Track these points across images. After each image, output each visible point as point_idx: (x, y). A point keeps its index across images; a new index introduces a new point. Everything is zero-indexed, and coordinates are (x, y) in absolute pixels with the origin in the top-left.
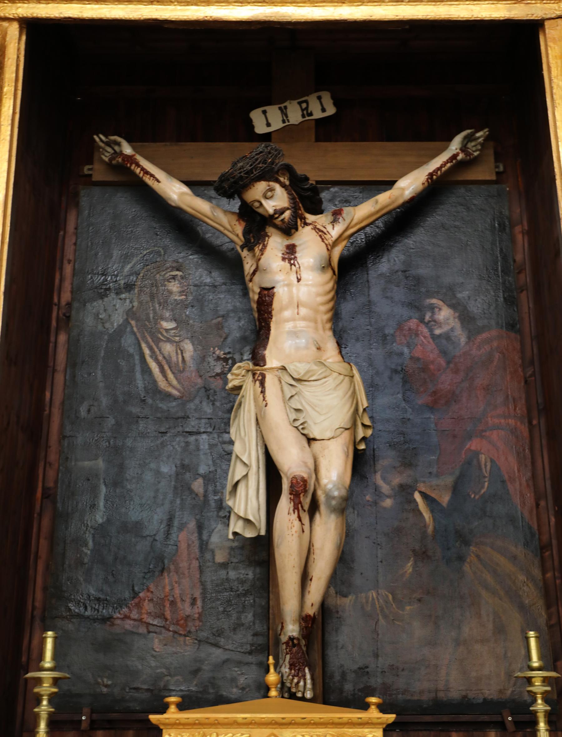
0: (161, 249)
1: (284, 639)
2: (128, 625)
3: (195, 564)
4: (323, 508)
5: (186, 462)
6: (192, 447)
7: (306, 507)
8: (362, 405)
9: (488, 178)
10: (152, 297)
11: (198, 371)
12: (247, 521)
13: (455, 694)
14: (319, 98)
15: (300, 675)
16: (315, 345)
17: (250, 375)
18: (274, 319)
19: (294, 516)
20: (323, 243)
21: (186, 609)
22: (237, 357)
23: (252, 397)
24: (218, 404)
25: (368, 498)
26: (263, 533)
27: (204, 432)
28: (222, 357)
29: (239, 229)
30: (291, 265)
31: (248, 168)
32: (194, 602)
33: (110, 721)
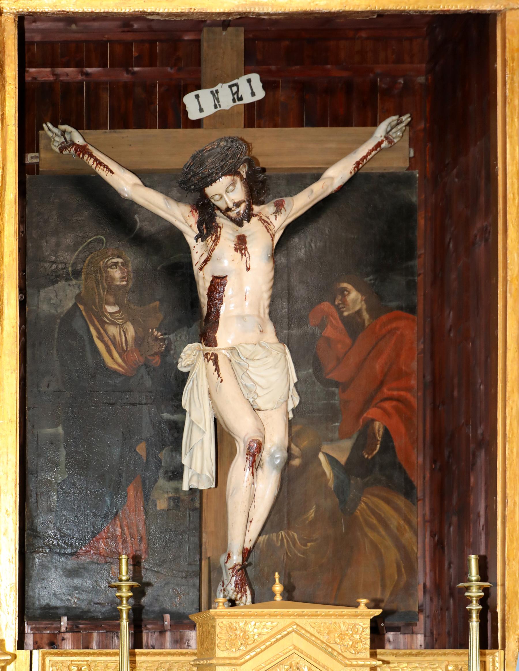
0: (103, 237)
8: (293, 380)
15: (243, 591)
16: (259, 328)
20: (268, 233)
23: (204, 374)
27: (145, 404)
28: (160, 337)
30: (242, 255)
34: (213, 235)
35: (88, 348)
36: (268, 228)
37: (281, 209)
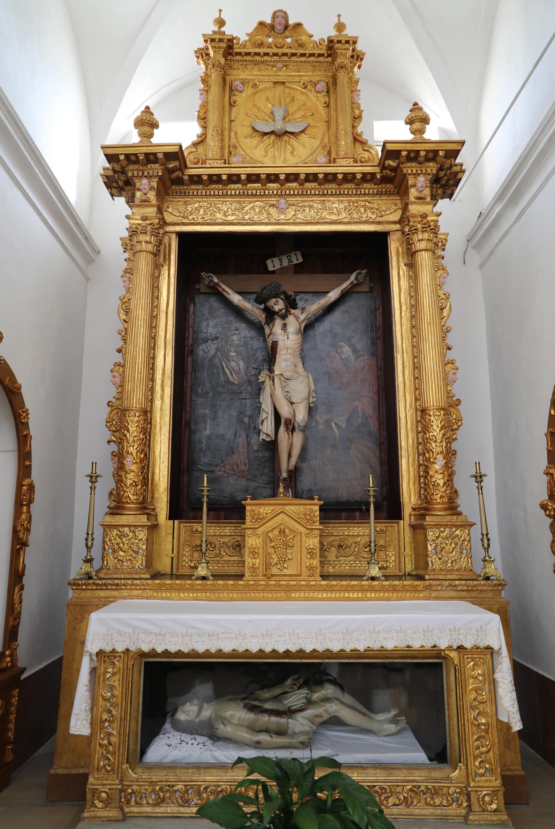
1: (281, 478)
2: (221, 473)
3: (246, 450)
4: (297, 430)
5: (241, 411)
6: (243, 405)
7: (291, 429)
9: (366, 290)
10: (226, 342)
11: (245, 373)
12: (267, 435)
13: (344, 499)
14: (296, 254)
17: (268, 377)
19: (286, 433)
21: (243, 468)
22: (261, 367)
24: (254, 387)
25: (313, 425)
26: (273, 439)
29: (264, 316)
31: (268, 293)
32: (245, 465)
33: (215, 508)
35: (221, 372)
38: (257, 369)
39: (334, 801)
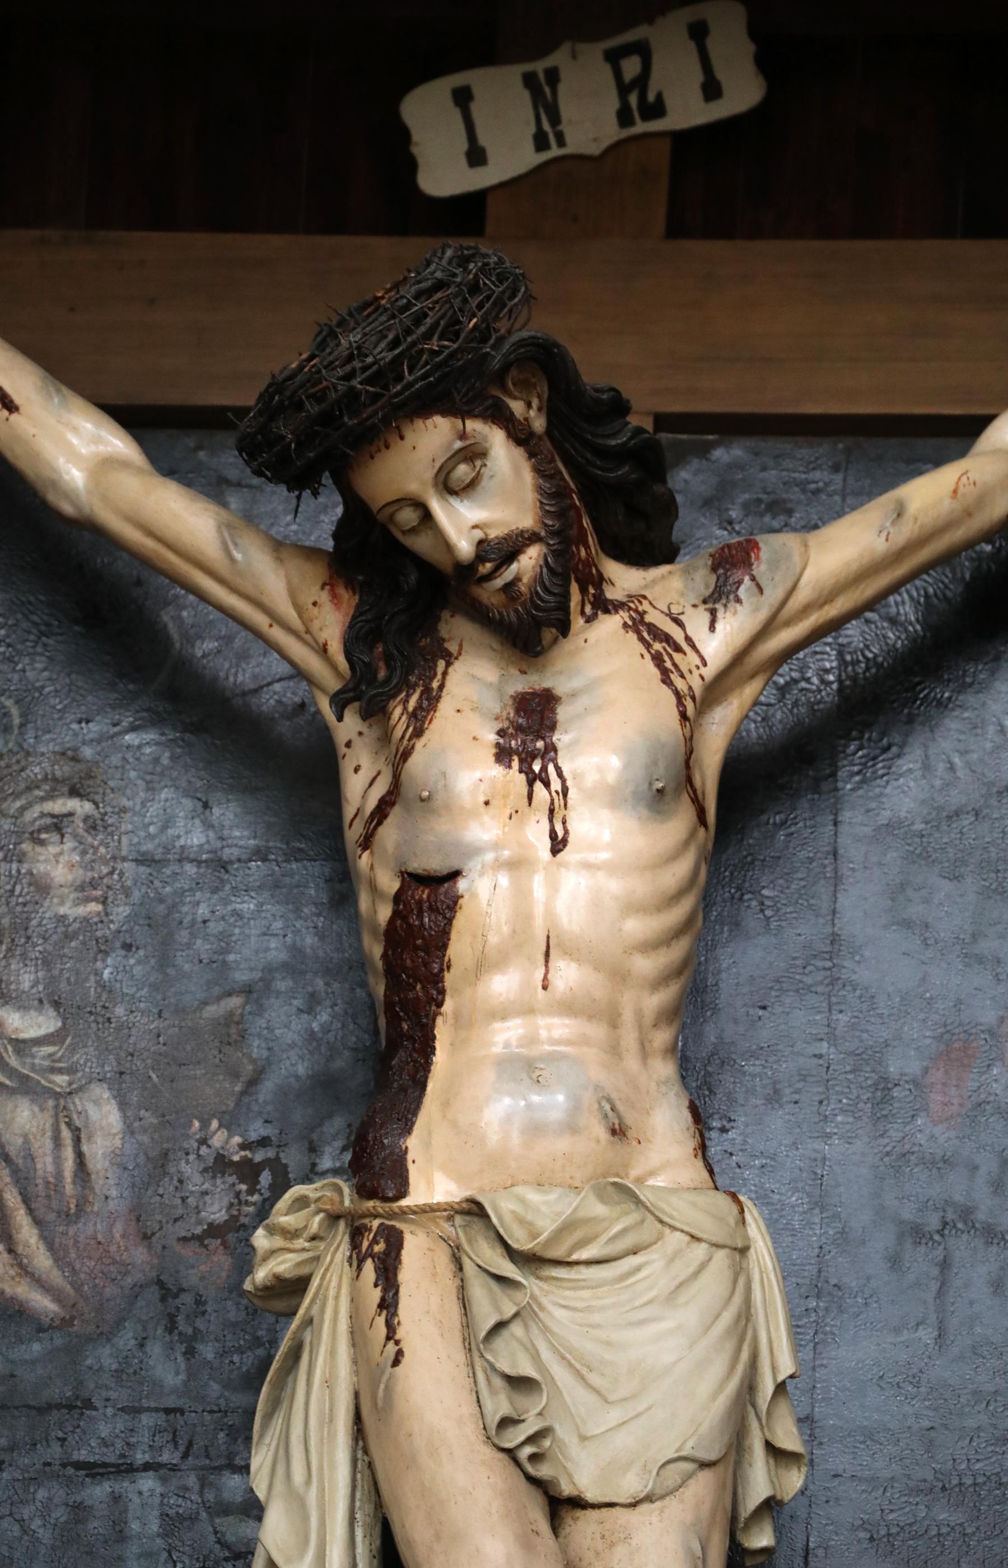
6: (96, 1526)
8: (774, 1369)
11: (137, 1214)
14: (699, 32)
18: (448, 1006)
22: (293, 1158)
24: (208, 1351)
27: (147, 1467)
31: (382, 353)
34: (413, 687)
36: (668, 664)
37: (740, 583)
38: (248, 1171)
39: (906, 639)
